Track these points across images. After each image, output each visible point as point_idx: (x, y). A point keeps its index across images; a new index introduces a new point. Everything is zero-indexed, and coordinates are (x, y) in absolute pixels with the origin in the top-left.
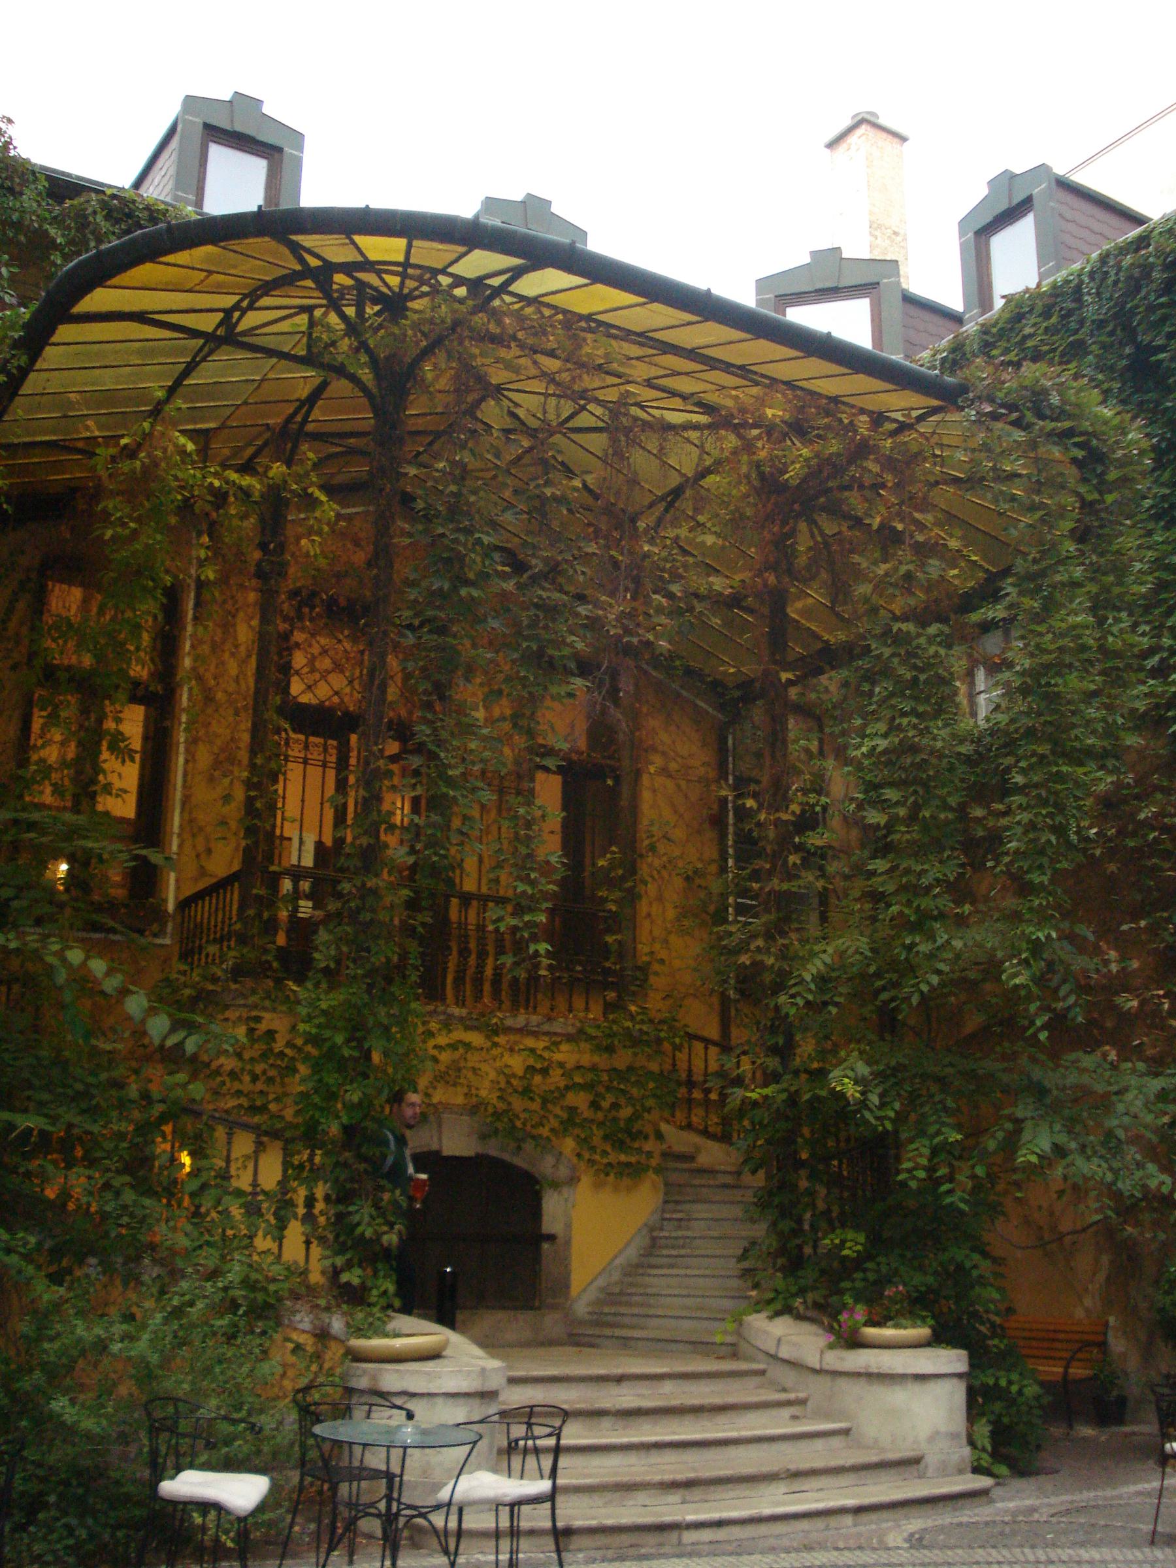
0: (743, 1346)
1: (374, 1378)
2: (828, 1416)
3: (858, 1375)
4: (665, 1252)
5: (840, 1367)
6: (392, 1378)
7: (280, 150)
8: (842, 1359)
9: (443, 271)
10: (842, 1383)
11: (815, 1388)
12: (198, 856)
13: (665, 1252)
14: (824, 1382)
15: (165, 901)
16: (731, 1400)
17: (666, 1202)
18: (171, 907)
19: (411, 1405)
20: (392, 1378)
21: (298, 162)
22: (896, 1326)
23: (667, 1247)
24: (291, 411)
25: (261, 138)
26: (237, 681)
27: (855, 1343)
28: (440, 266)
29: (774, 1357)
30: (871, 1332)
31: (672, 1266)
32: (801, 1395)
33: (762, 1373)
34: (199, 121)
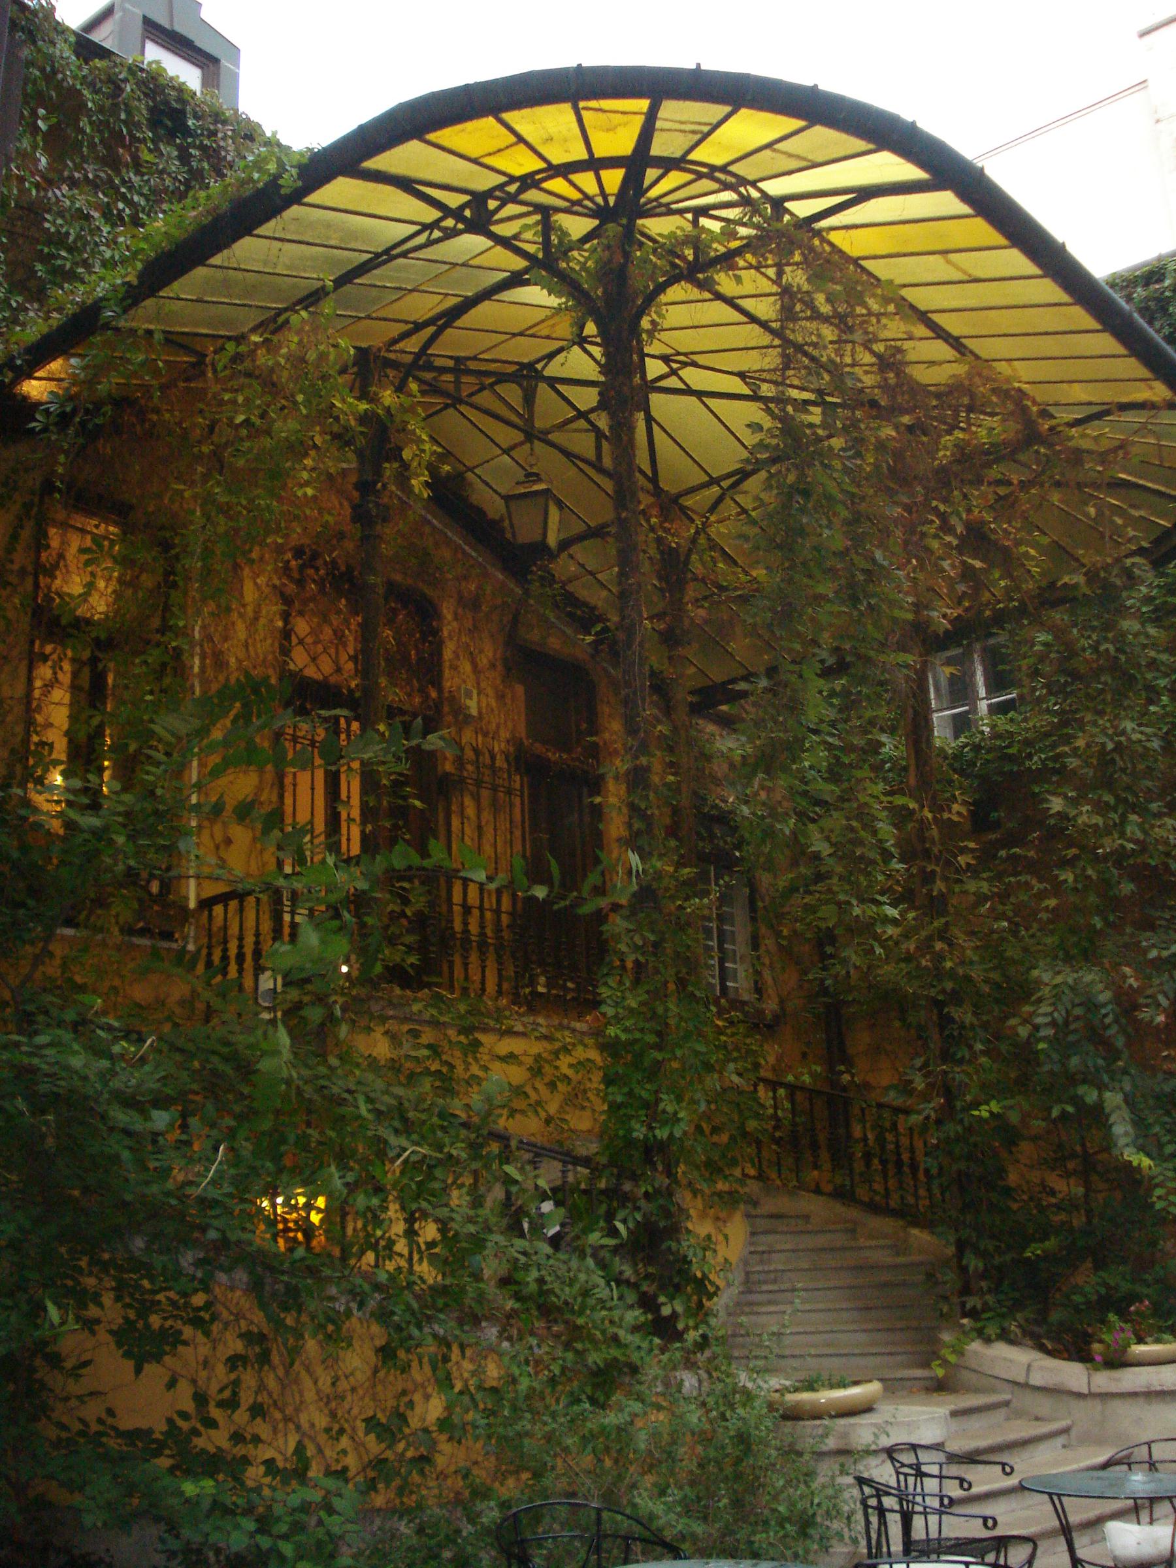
0: (965, 1375)
1: (845, 1435)
2: (1100, 1442)
3: (1134, 1395)
4: (765, 1288)
5: (1113, 1388)
6: (836, 1433)
7: (216, 61)
8: (1118, 1380)
9: (754, 184)
10: (1116, 1404)
11: (1081, 1415)
12: (217, 847)
13: (765, 1288)
14: (1096, 1406)
15: (187, 898)
16: (1012, 1436)
17: (753, 1234)
18: (192, 904)
19: (1005, 1458)
20: (836, 1433)
21: (235, 77)
22: (1158, 1341)
23: (766, 1282)
24: (395, 334)
25: (198, 43)
26: (246, 646)
27: (1117, 1361)
28: (750, 178)
29: (1026, 1386)
30: (1139, 1349)
31: (770, 1303)
32: (1063, 1424)
33: (1007, 1404)
34: (139, 12)
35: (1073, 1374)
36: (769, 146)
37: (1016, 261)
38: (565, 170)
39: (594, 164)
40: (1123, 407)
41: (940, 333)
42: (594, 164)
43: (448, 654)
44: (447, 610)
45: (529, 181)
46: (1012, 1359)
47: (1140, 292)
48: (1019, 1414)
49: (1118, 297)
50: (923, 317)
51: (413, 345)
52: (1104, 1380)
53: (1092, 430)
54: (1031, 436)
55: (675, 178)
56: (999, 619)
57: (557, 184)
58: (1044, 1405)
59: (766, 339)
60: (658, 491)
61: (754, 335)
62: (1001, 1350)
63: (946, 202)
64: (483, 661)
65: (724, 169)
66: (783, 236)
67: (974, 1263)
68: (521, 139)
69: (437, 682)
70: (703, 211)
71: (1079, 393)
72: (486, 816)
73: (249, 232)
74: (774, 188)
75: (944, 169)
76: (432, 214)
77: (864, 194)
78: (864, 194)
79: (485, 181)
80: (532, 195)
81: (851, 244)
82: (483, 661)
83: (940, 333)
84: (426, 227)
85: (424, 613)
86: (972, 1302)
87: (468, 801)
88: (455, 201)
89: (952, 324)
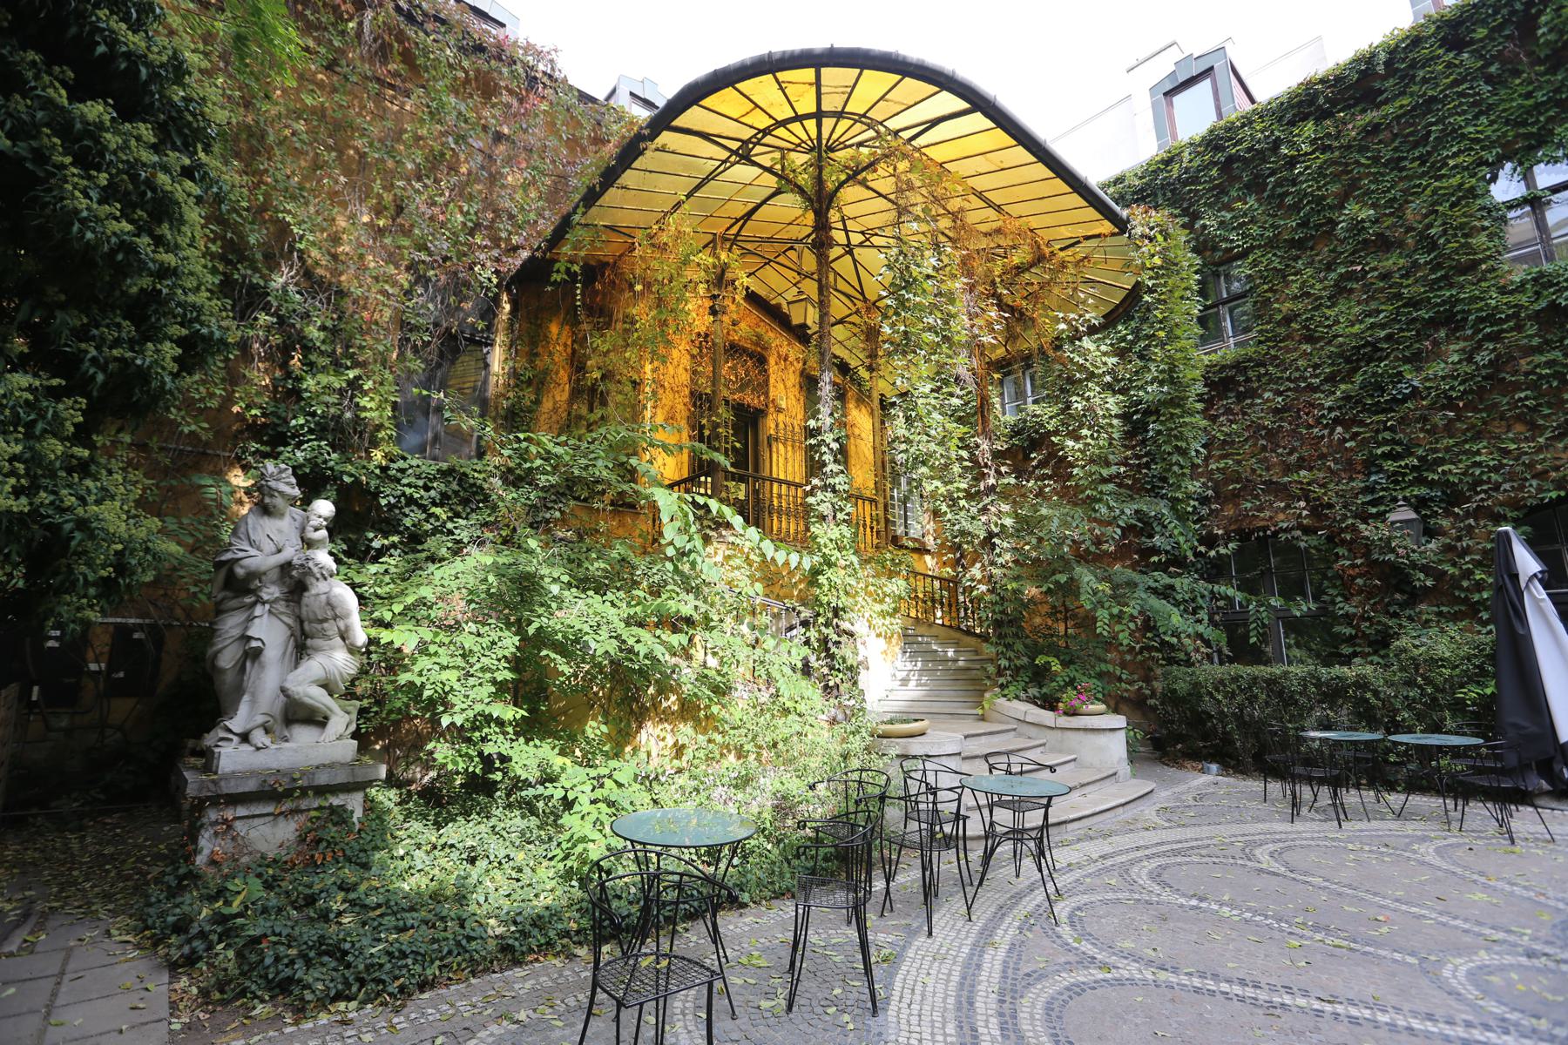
2: (1060, 751)
27: (1073, 713)
35: (1047, 717)
36: (882, 98)
37: (1022, 155)
38: (783, 123)
39: (798, 118)
40: (1087, 238)
41: (990, 204)
42: (798, 118)
43: (772, 381)
44: (772, 361)
45: (766, 132)
46: (1021, 708)
47: (1111, 190)
48: (1020, 735)
49: (1101, 193)
50: (980, 195)
51: (734, 230)
52: (1064, 721)
53: (1069, 252)
54: (1039, 259)
55: (844, 124)
56: (823, 262)
57: (781, 132)
58: (1033, 731)
59: (890, 205)
60: (865, 300)
61: (882, 204)
62: (1016, 704)
63: (978, 120)
64: (789, 384)
65: (864, 116)
66: (896, 148)
67: (1004, 663)
68: (757, 106)
69: (767, 394)
70: (860, 144)
71: (1066, 232)
72: (790, 454)
73: (629, 167)
74: (893, 124)
75: (978, 102)
76: (724, 154)
77: (935, 122)
78: (935, 122)
79: (747, 133)
80: (768, 139)
81: (937, 154)
82: (789, 384)
83: (990, 204)
84: (724, 162)
85: (761, 361)
86: (1002, 680)
87: (781, 446)
88: (734, 145)
89: (995, 197)
